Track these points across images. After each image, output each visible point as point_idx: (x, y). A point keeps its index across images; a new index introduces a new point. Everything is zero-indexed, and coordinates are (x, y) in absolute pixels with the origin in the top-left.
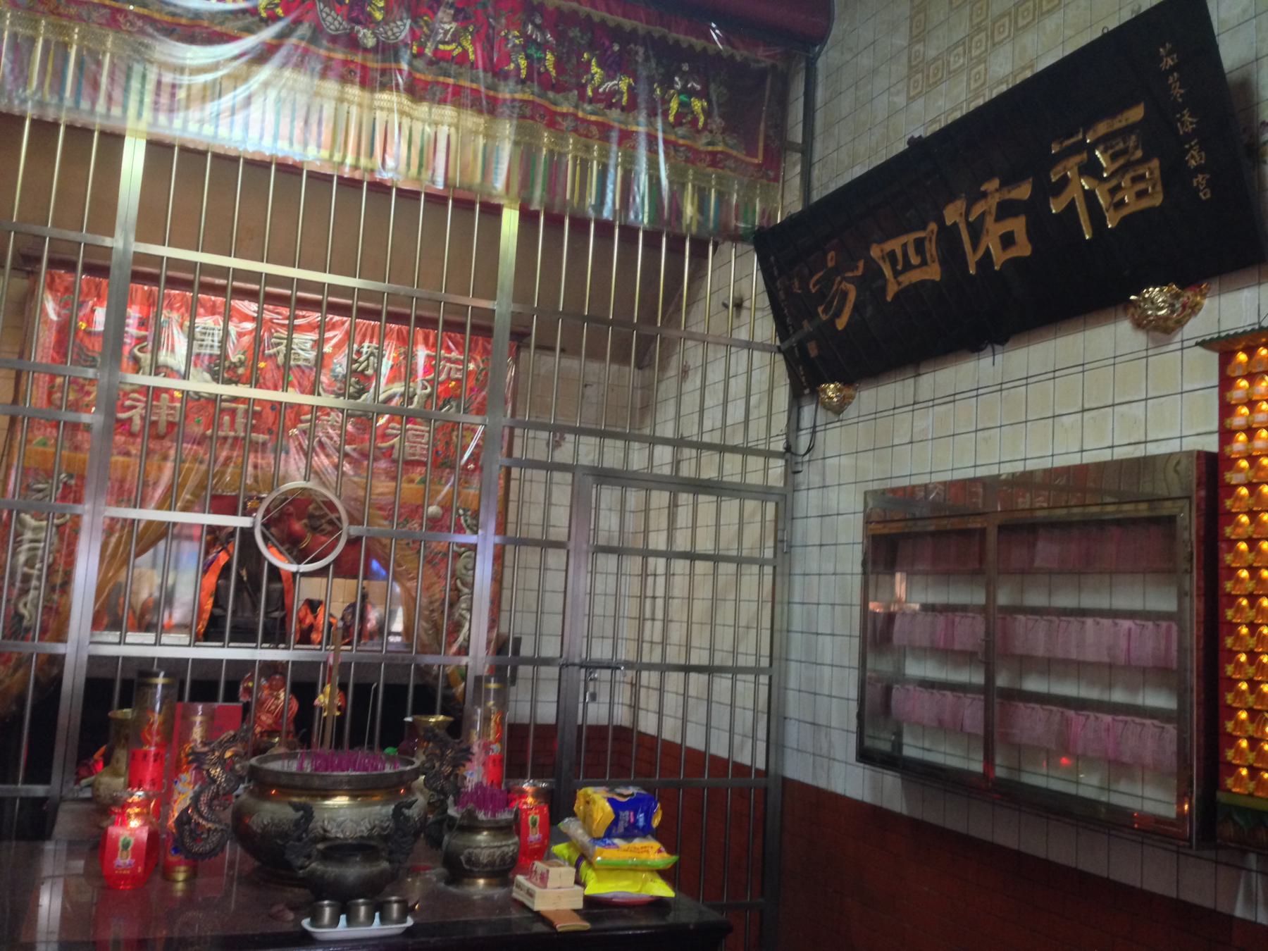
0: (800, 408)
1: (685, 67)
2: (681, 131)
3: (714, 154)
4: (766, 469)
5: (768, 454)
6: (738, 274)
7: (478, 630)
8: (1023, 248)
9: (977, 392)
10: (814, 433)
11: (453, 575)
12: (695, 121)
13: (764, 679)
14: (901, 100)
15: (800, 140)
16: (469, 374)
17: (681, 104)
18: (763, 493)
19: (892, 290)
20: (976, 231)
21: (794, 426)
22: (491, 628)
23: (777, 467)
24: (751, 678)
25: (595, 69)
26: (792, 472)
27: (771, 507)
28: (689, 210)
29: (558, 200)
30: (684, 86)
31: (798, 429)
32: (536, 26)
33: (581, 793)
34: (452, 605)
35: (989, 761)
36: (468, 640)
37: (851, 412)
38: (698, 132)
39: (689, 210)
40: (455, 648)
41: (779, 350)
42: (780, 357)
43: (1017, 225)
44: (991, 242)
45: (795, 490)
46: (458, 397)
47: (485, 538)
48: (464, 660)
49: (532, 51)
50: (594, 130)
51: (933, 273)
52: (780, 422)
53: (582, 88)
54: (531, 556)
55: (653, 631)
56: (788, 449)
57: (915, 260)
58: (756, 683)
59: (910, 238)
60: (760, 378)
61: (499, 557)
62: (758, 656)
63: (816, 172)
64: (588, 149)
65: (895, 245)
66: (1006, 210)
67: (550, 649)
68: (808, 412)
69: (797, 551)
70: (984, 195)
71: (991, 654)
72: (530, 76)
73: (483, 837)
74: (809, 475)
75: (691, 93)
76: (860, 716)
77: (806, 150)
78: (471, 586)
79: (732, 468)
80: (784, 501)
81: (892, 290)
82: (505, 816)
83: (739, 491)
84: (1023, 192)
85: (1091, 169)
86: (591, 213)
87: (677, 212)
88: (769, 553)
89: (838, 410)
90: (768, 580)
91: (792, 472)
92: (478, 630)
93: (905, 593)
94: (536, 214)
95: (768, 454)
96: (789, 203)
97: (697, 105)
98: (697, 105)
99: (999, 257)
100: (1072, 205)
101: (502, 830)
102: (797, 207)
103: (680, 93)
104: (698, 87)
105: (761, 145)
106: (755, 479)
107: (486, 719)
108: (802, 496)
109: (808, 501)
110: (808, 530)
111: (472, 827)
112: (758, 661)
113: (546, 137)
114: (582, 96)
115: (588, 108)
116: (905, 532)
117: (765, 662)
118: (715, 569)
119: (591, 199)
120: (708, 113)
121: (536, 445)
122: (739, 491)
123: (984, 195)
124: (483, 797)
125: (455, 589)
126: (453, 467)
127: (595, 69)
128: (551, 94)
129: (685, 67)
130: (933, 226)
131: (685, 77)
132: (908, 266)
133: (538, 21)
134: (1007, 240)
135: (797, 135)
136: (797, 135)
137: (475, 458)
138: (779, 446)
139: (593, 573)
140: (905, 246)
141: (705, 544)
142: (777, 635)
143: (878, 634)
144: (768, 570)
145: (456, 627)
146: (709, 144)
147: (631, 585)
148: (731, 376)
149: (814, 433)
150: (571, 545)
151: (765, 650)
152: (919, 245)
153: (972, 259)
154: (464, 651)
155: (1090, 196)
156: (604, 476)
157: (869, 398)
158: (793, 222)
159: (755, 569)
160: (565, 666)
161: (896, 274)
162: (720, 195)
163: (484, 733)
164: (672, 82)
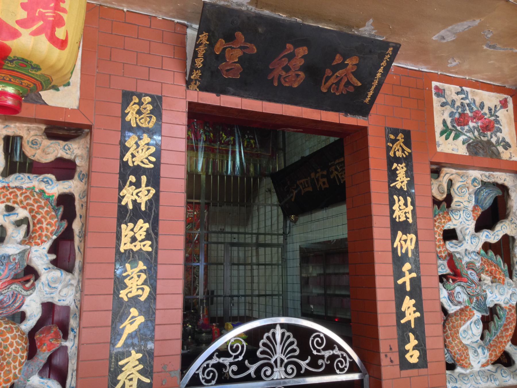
0: (286, 221)
1: (248, 132)
2: (248, 149)
3: (257, 154)
4: (278, 239)
5: (278, 235)
6: (267, 183)
7: (201, 289)
8: (327, 186)
9: (323, 219)
10: (290, 228)
11: (194, 274)
12: (252, 146)
13: (281, 297)
14: (304, 141)
15: (282, 147)
16: (195, 215)
17: (248, 142)
18: (277, 245)
19: (303, 192)
20: (318, 180)
21: (285, 227)
22: (204, 289)
23: (281, 238)
24: (277, 297)
25: (223, 135)
26: (285, 239)
27: (280, 249)
28: (252, 169)
29: (216, 171)
30: (248, 137)
31: (286, 227)
32: (208, 127)
33: (226, 324)
34: (194, 282)
35: (326, 313)
36: (198, 292)
37: (298, 223)
38: (253, 148)
39: (252, 169)
40: (195, 295)
41: (280, 205)
42: (280, 207)
43: (325, 180)
44: (321, 183)
45: (287, 244)
46: (192, 222)
47: (201, 263)
48: (198, 297)
49: (207, 134)
50: (224, 151)
51: (310, 189)
52: (281, 225)
53: (220, 141)
54: (213, 267)
55: (255, 286)
56: (284, 233)
57: (307, 186)
58: (279, 299)
59: (305, 180)
60: (275, 212)
61: (206, 268)
62: (279, 291)
63: (287, 156)
64: (223, 157)
65: (302, 181)
66: (323, 176)
67: (221, 293)
68: (288, 222)
69: (288, 261)
70: (318, 172)
71: (326, 286)
72: (206, 140)
73: (204, 335)
74: (289, 240)
75: (250, 138)
76: (301, 304)
77: (284, 150)
78: (198, 276)
79: (268, 239)
80: (284, 247)
81: (303, 192)
82: (209, 330)
83: (271, 245)
84: (325, 173)
85: (336, 170)
86: (225, 174)
87: (248, 170)
88: (280, 262)
89: (295, 222)
90: (280, 269)
91: (285, 239)
92: (201, 289)
93: (314, 271)
94: (210, 176)
95: (278, 235)
96: (279, 166)
97: (252, 141)
98: (252, 141)
99: (323, 187)
100: (334, 177)
101: (208, 333)
102: (283, 167)
103: (247, 139)
104: (252, 137)
105: (271, 150)
106: (275, 241)
107: (203, 309)
108: (288, 246)
109: (290, 247)
110: (290, 255)
111: (201, 332)
112: (279, 292)
113: (212, 156)
114: (221, 143)
115: (223, 146)
116: (308, 255)
117: (281, 293)
118: (265, 267)
119: (225, 170)
120: (255, 143)
121: (213, 238)
122: (271, 245)
123: (318, 172)
124: (204, 326)
125: (194, 278)
126: (192, 243)
127: (223, 135)
128: (212, 144)
129: (248, 132)
130: (309, 178)
131: (248, 135)
132: (305, 187)
133: (208, 125)
134: (324, 183)
135: (281, 146)
136: (281, 146)
137: (198, 239)
138: (281, 232)
139: (231, 270)
140: (304, 182)
141: (268, 261)
142: (284, 285)
143: (305, 282)
144: (280, 267)
145: (195, 289)
146: (256, 151)
147: (249, 273)
148: (268, 213)
149: (290, 228)
150: (225, 264)
151: (281, 290)
152: (307, 182)
153: (318, 187)
154: (198, 294)
155: (337, 175)
156: (233, 244)
157: (302, 219)
158: (281, 171)
159: (277, 267)
160: (225, 297)
161: (303, 189)
162: (260, 165)
163: (203, 312)
164: (245, 137)
